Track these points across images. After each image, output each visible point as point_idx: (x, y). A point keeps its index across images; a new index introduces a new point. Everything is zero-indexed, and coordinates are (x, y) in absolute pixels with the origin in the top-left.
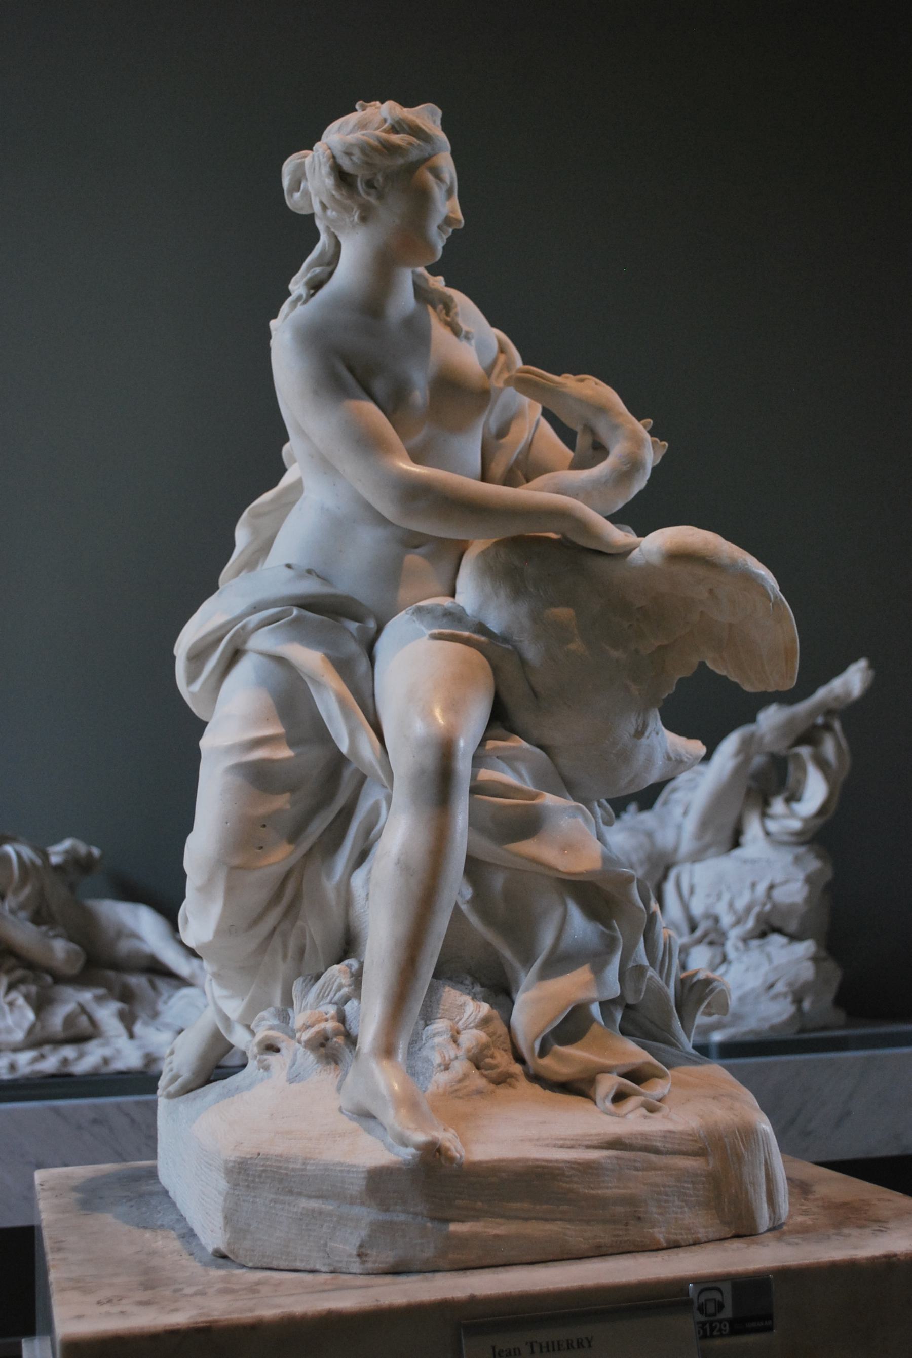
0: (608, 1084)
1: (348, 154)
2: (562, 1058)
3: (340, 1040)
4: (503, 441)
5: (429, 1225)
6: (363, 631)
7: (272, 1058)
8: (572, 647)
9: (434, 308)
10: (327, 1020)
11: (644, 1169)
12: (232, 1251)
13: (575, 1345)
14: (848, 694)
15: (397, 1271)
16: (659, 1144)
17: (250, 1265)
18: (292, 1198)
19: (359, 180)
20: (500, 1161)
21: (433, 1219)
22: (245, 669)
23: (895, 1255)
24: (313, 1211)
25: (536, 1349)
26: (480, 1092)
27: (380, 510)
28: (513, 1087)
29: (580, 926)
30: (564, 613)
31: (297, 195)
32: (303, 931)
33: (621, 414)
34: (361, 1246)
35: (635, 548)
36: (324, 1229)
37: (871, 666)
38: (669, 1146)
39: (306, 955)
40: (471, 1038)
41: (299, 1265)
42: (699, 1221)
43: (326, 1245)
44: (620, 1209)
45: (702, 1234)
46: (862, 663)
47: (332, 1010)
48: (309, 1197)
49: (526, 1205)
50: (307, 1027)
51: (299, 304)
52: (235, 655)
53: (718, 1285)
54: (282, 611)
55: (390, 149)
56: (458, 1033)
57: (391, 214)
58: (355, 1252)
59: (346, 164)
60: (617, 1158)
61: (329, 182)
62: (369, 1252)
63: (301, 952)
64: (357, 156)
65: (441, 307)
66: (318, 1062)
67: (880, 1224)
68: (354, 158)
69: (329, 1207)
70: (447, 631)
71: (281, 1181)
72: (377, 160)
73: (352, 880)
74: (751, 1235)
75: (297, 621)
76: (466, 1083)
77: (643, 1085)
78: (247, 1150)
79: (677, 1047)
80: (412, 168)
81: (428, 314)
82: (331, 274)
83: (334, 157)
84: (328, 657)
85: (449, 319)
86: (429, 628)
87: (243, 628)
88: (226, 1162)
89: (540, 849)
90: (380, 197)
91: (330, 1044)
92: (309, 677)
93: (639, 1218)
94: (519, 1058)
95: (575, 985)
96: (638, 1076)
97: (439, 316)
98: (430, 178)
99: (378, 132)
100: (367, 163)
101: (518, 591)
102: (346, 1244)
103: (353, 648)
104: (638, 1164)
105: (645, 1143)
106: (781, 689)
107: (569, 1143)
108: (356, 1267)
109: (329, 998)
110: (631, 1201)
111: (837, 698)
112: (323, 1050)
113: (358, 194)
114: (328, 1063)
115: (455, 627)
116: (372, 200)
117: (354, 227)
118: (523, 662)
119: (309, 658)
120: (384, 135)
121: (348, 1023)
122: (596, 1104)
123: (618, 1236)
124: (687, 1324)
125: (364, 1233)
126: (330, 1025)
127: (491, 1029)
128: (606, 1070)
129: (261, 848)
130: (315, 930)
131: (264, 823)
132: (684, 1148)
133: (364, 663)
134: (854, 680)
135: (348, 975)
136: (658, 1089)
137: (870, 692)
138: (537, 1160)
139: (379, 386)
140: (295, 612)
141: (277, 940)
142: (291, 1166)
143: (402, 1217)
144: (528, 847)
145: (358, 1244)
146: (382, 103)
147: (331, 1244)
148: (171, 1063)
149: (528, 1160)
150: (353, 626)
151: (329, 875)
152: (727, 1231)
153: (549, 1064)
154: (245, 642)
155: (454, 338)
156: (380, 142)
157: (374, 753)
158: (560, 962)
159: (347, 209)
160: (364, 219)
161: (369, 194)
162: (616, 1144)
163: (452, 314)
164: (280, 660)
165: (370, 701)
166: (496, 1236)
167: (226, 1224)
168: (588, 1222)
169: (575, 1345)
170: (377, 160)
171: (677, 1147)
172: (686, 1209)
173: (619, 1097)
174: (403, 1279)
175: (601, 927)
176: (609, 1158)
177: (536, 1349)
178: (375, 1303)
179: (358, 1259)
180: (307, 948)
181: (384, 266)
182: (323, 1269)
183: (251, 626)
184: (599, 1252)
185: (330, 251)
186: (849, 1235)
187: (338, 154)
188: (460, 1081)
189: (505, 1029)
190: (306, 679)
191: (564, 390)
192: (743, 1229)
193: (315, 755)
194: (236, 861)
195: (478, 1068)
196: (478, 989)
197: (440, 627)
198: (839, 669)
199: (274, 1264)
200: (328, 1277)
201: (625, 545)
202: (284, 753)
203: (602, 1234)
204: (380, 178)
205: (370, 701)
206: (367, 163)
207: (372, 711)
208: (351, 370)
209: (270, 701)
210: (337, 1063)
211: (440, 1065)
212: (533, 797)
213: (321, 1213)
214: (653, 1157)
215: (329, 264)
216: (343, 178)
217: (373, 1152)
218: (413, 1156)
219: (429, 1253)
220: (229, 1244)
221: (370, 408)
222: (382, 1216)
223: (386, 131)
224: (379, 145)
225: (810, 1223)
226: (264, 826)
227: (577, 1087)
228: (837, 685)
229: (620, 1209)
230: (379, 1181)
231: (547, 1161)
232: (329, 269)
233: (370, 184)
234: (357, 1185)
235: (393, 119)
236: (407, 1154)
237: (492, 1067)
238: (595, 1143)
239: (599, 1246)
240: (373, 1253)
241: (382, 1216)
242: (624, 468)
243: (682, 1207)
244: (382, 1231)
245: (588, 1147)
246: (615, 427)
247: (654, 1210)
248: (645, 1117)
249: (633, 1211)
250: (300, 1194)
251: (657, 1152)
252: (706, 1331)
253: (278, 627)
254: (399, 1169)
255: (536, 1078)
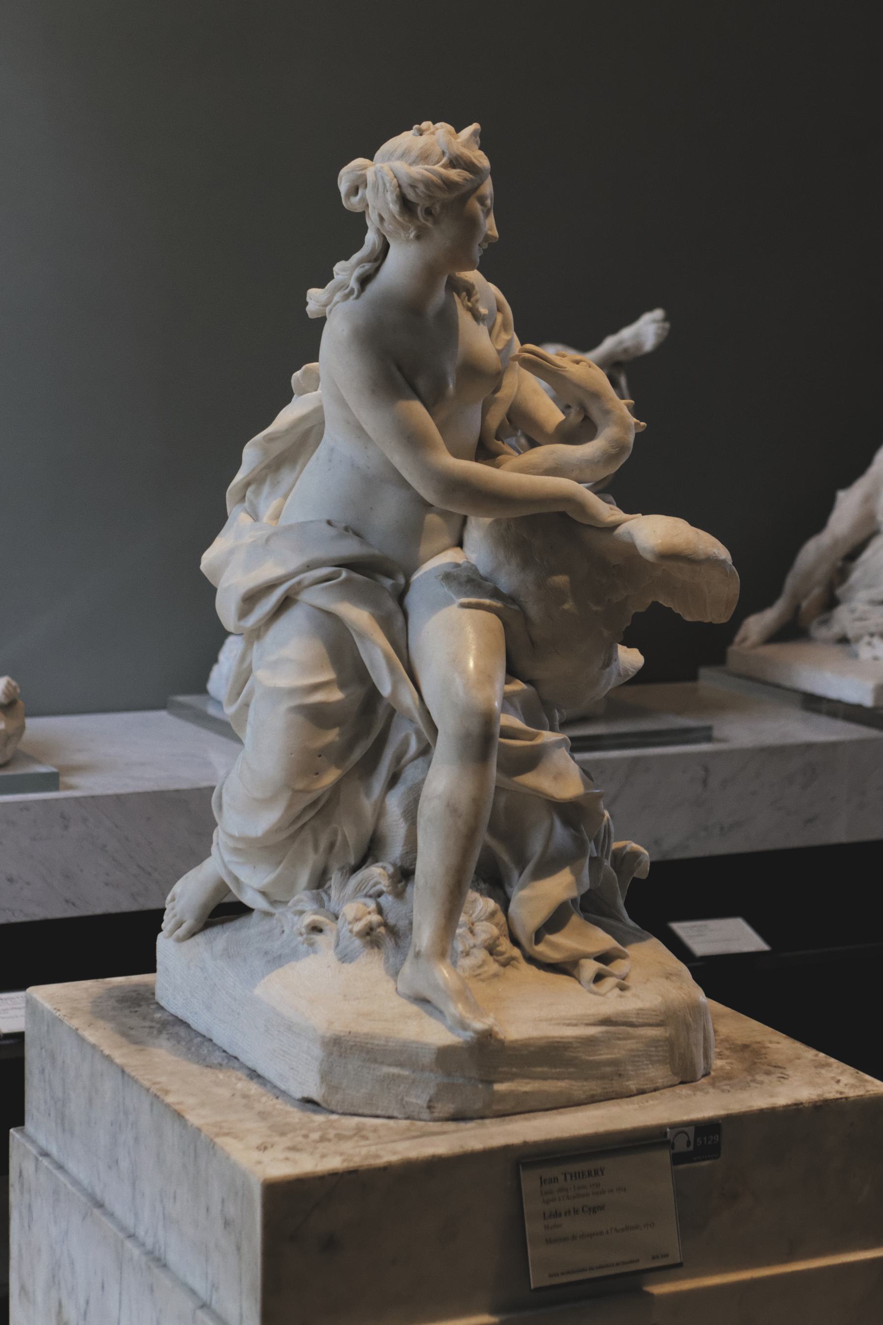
0: (590, 967)
1: (413, 187)
2: (554, 946)
3: (382, 930)
4: (498, 395)
5: (480, 1086)
6: (394, 586)
7: (318, 938)
8: (566, 606)
9: (459, 296)
10: (369, 913)
11: (624, 1039)
12: (326, 1101)
13: (593, 1173)
14: (639, 346)
15: (458, 1117)
16: (634, 1020)
17: (341, 1111)
18: (376, 1066)
19: (419, 209)
20: (530, 1039)
21: (482, 1081)
22: (296, 617)
23: (802, 1103)
24: (393, 1075)
25: (568, 1177)
26: (496, 975)
27: (398, 468)
28: (517, 968)
29: (561, 834)
30: (561, 580)
31: (355, 200)
32: (335, 833)
33: (611, 399)
34: (430, 1101)
35: (619, 525)
36: (401, 1088)
37: (666, 319)
38: (640, 1020)
39: (336, 849)
40: (487, 930)
41: (379, 1112)
42: (657, 1073)
43: (402, 1099)
44: (608, 1069)
45: (660, 1082)
46: (658, 314)
47: (372, 905)
48: (390, 1065)
49: (546, 1069)
50: (357, 920)
51: (352, 298)
52: (286, 603)
53: (686, 1129)
54: (334, 572)
55: (449, 185)
56: (473, 924)
57: (443, 236)
58: (425, 1105)
59: (411, 195)
60: (607, 1032)
61: (394, 208)
62: (436, 1105)
63: (332, 845)
64: (421, 188)
65: (464, 294)
66: (364, 946)
67: (781, 1070)
68: (418, 191)
69: (405, 1072)
70: (473, 600)
71: (368, 1052)
72: (439, 195)
73: (386, 799)
74: (692, 1082)
75: (347, 581)
76: (486, 968)
77: (611, 965)
78: (339, 1028)
79: (621, 921)
80: (464, 199)
81: (455, 302)
82: (377, 270)
83: (399, 186)
84: (373, 615)
85: (470, 304)
86: (460, 594)
87: (299, 583)
88: (323, 1037)
89: (537, 780)
90: (436, 222)
91: (374, 933)
92: (355, 631)
93: (620, 1075)
94: (515, 942)
95: (560, 886)
96: (605, 958)
97: (462, 301)
98: (478, 206)
99: (437, 168)
100: (430, 197)
101: (526, 563)
102: (418, 1099)
103: (391, 604)
104: (620, 1036)
105: (625, 1020)
106: (714, 622)
107: (574, 1022)
108: (426, 1115)
109: (365, 891)
110: (614, 1063)
111: (626, 351)
112: (368, 938)
113: (417, 218)
114: (372, 948)
115: (469, 582)
116: (429, 224)
117: (408, 240)
118: (526, 619)
119: (358, 616)
120: (443, 171)
121: (385, 914)
122: (580, 982)
123: (605, 1088)
124: (664, 1156)
125: (432, 1091)
126: (375, 918)
127: (496, 920)
128: (586, 956)
129: (317, 774)
130: (350, 834)
131: (321, 753)
132: (650, 1021)
133: (400, 618)
134: (646, 330)
135: (387, 878)
136: (619, 967)
137: (662, 347)
138: (554, 1037)
139: (422, 383)
140: (344, 574)
141: (307, 834)
142: (376, 1042)
143: (461, 1081)
144: (529, 779)
145: (428, 1099)
146: (434, 123)
147: (406, 1099)
148: (173, 909)
149: (549, 1038)
150: (388, 582)
151: (368, 794)
152: (677, 1079)
153: (541, 949)
154: (297, 593)
155: (474, 323)
156: (443, 181)
157: (415, 703)
158: (547, 868)
159: (406, 229)
160: (418, 237)
161: (426, 220)
162: (606, 1021)
163: (472, 299)
164: (329, 614)
165: (404, 651)
166: (526, 1093)
167: (322, 1082)
168: (586, 1079)
169: (593, 1173)
170: (439, 195)
171: (646, 1021)
172: (650, 1066)
173: (599, 978)
174: (462, 1125)
175: (573, 831)
176: (602, 1032)
177: (568, 1177)
178: (461, 1150)
179: (427, 1110)
180: (338, 844)
181: (438, 275)
182: (400, 1116)
183: (306, 583)
184: (592, 1100)
185: (378, 247)
186: (762, 1083)
187: (404, 185)
188: (480, 967)
189: (504, 919)
190: (352, 631)
191: (563, 373)
192: (686, 1075)
193: (359, 692)
194: (300, 786)
195: (491, 954)
196: (483, 886)
197: (467, 596)
198: (631, 318)
199: (360, 1111)
200: (405, 1123)
201: (612, 522)
202: (336, 695)
203: (593, 1087)
204: (438, 207)
205: (404, 651)
206: (430, 197)
207: (406, 657)
208: (400, 369)
209: (324, 651)
210: (379, 948)
211: (462, 952)
212: (533, 737)
213: (399, 1076)
214: (630, 1030)
215: (376, 260)
216: (406, 205)
217: (436, 1034)
218: (472, 1038)
219: (479, 1105)
220: (323, 1096)
221: (417, 407)
222: (446, 1080)
223: (444, 166)
224: (439, 181)
225: (728, 1068)
226: (320, 756)
227: (564, 968)
228: (627, 334)
229: (608, 1069)
230: (445, 1056)
231: (561, 1038)
232: (376, 264)
233: (428, 212)
234: (428, 1059)
235: (450, 154)
236: (468, 1035)
237: (502, 954)
238: (592, 1021)
239: (593, 1096)
240: (439, 1106)
241: (446, 1080)
242: (613, 451)
243: (647, 1065)
244: (444, 1091)
245: (588, 1025)
246: (607, 412)
247: (630, 1068)
248: (621, 996)
249: (617, 1070)
250: (382, 1063)
251: (632, 1025)
252: (678, 1159)
253: (331, 586)
254: (462, 1048)
255: (531, 960)
